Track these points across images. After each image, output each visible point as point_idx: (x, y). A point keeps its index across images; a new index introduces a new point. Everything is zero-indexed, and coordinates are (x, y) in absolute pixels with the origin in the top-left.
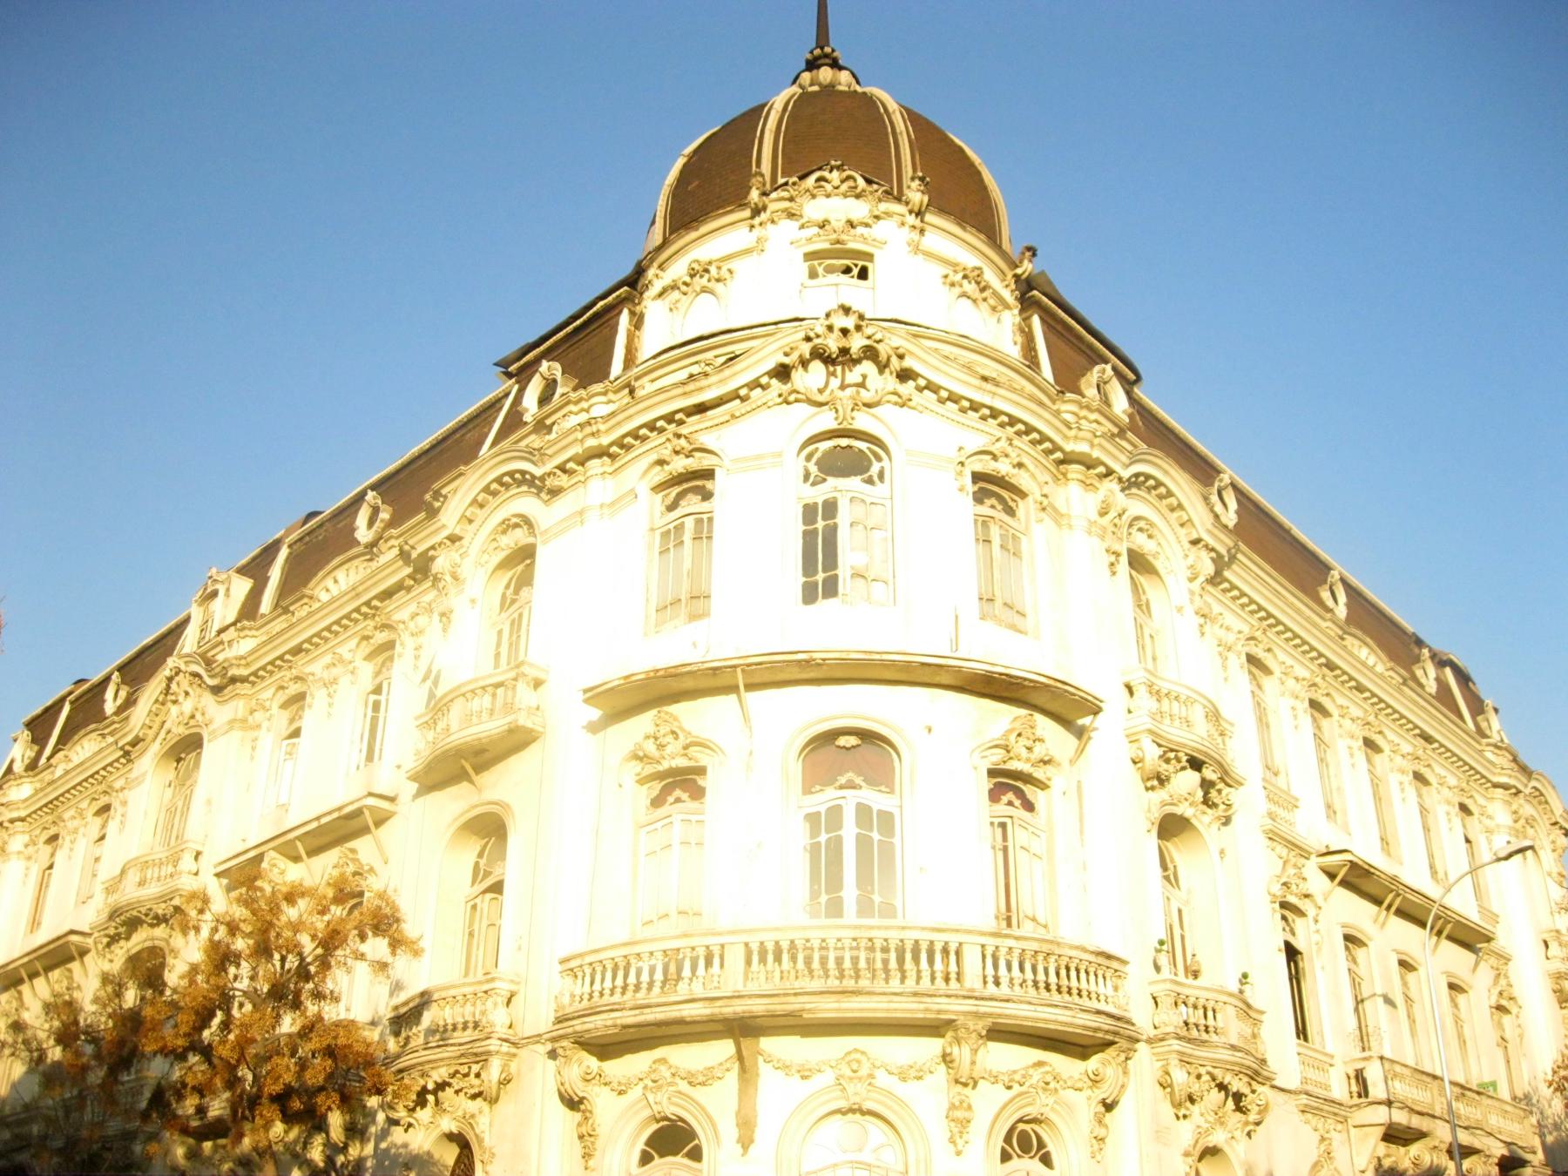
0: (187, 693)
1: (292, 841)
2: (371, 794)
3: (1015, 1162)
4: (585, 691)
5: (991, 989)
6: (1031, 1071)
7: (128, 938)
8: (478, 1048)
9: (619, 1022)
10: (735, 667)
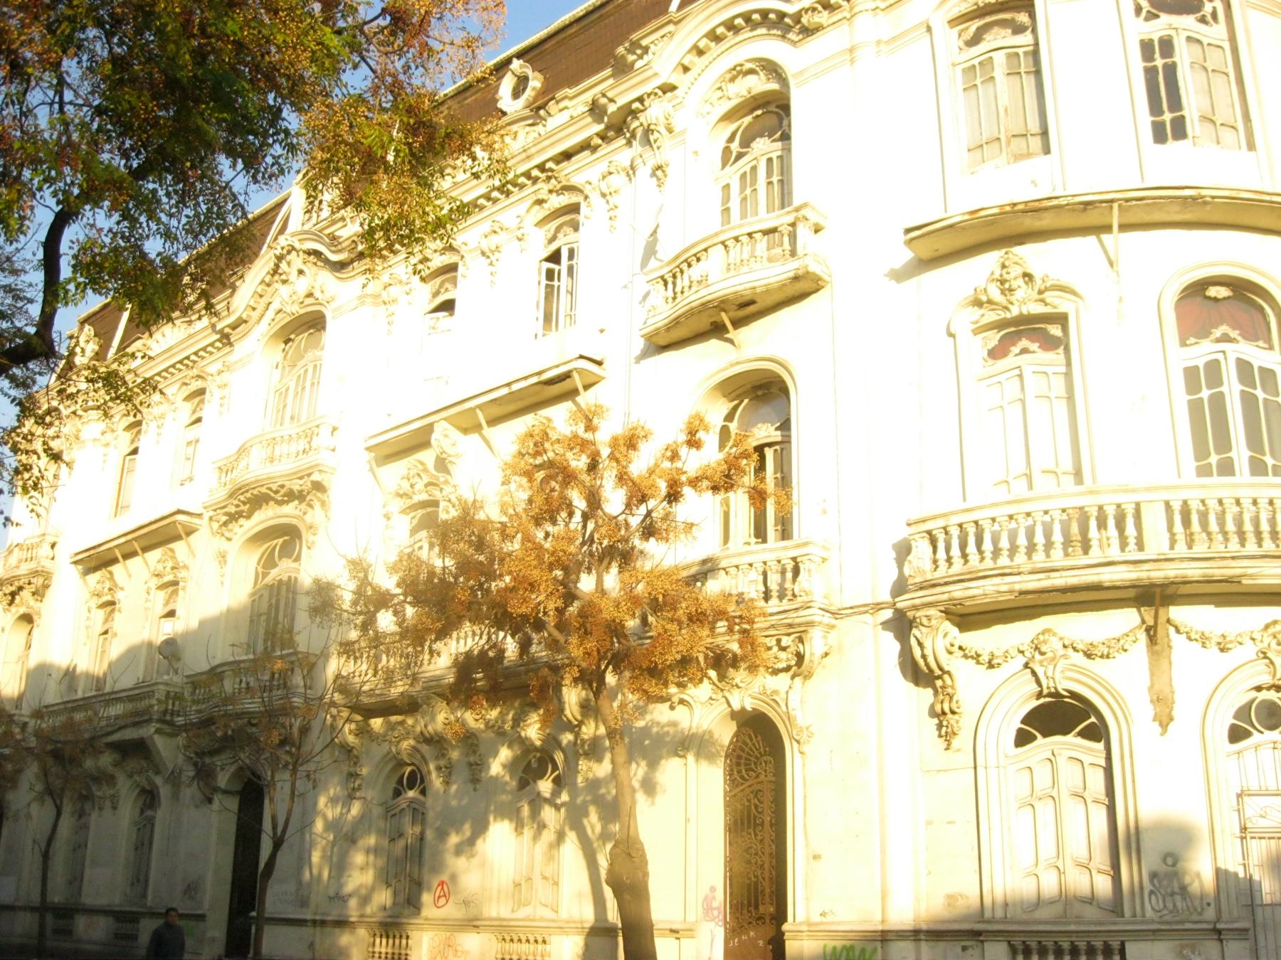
0: (301, 272)
1: (472, 410)
2: (582, 357)
4: (908, 231)
7: (248, 517)
8: (793, 618)
9: (1017, 587)
10: (1112, 201)
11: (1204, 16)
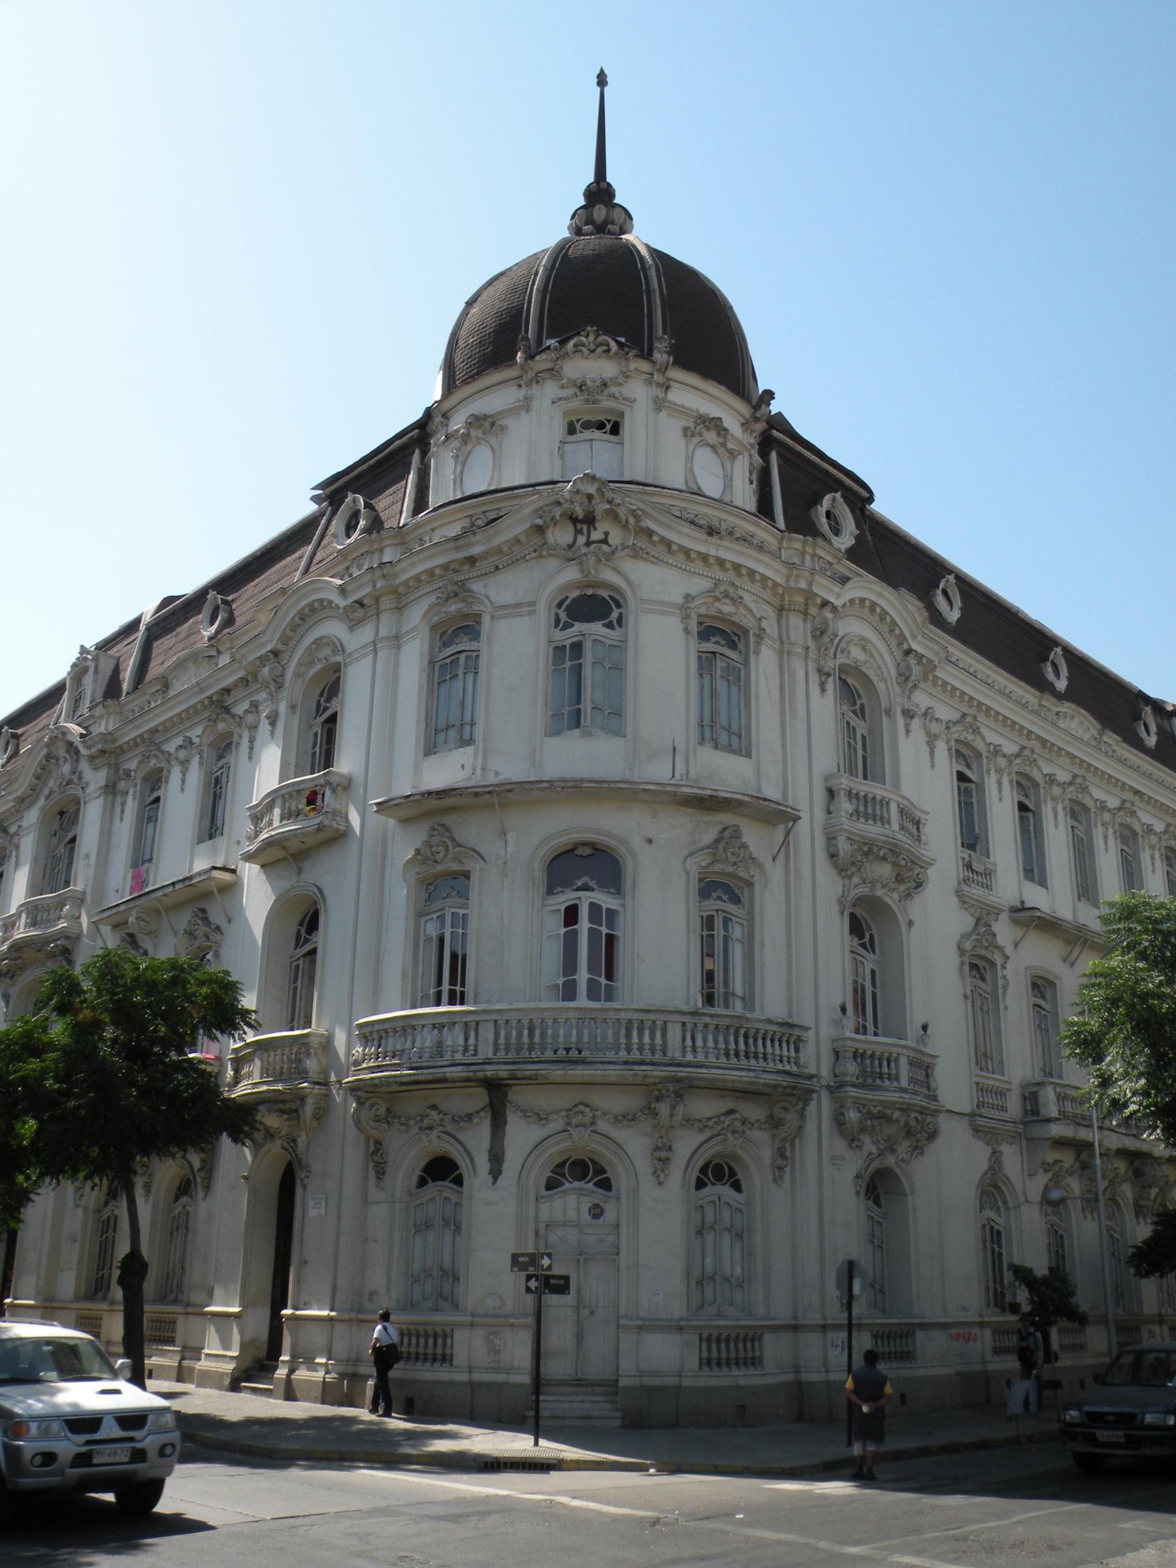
3: (709, 1189)
5: (689, 1057)
6: (722, 1118)
11: (611, 622)
